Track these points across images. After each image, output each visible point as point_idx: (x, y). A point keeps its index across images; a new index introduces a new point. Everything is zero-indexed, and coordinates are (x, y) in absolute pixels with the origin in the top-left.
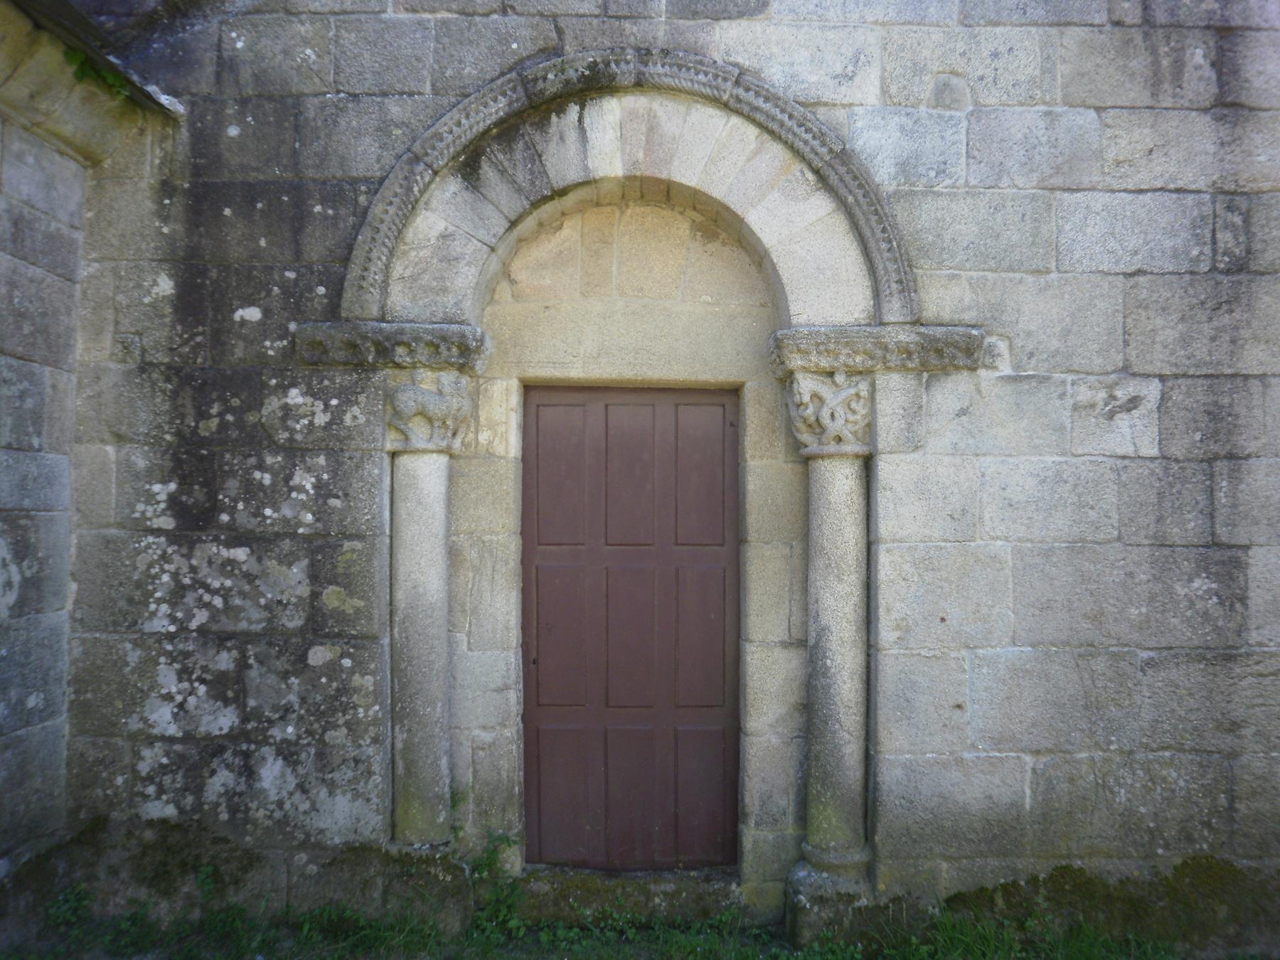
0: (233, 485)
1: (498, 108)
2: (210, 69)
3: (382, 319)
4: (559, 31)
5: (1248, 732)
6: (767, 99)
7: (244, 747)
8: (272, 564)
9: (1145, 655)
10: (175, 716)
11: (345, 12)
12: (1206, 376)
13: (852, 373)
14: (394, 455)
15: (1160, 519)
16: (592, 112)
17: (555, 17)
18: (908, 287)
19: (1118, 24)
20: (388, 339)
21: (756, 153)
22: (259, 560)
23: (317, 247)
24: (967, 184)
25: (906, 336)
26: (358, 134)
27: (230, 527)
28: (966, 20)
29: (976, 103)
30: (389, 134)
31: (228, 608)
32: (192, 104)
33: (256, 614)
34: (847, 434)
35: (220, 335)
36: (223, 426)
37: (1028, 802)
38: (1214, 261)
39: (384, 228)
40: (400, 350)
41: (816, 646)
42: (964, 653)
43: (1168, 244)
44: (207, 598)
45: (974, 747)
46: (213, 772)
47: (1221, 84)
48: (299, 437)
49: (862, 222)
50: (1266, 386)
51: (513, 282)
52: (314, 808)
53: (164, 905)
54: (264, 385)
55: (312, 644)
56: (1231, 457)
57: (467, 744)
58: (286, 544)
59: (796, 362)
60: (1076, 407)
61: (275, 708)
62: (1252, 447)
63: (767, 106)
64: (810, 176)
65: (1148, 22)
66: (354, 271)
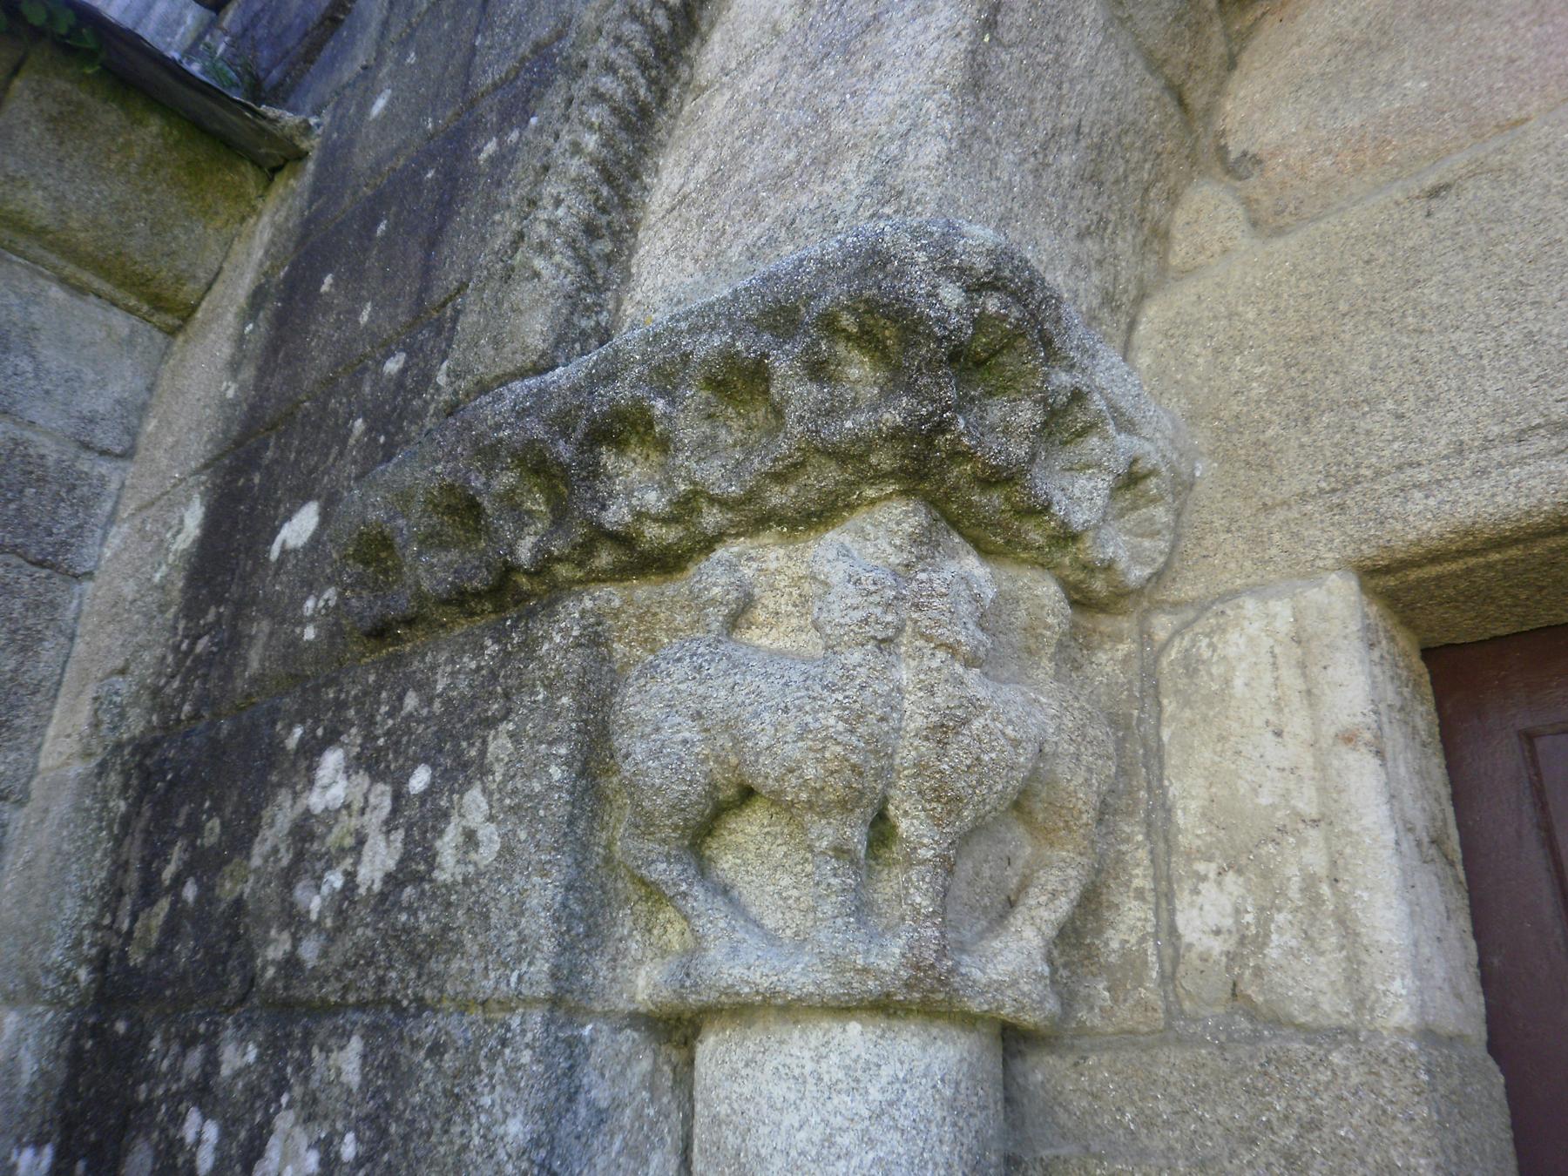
20: (563, 424)
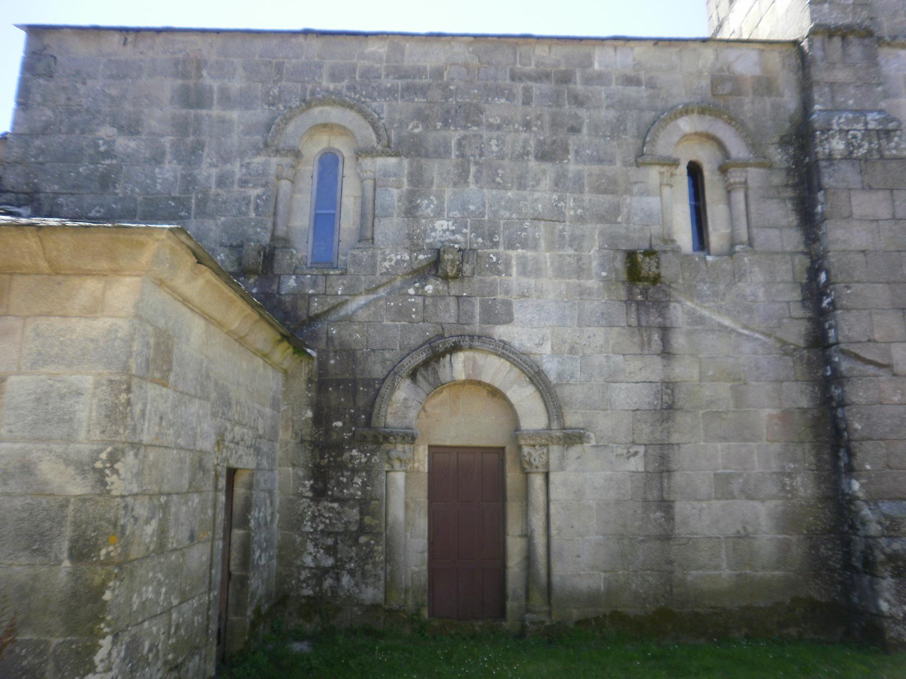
0: (333, 482)
1: (423, 357)
2: (324, 341)
3: (385, 427)
4: (443, 329)
5: (676, 564)
6: (513, 354)
7: (336, 571)
8: (346, 509)
9: (641, 538)
10: (313, 560)
11: (370, 322)
12: (660, 444)
13: (541, 445)
14: (387, 472)
15: (645, 493)
16: (454, 357)
17: (441, 324)
18: (560, 416)
19: (630, 326)
21: (509, 371)
22: (342, 507)
23: (361, 402)
24: (580, 381)
25: (559, 433)
26: (375, 363)
27: (332, 496)
28: (579, 325)
29: (583, 353)
30: (385, 363)
31: (331, 523)
32: (318, 353)
33: (340, 526)
34: (539, 465)
35: (328, 430)
36: (329, 462)
37: (602, 588)
38: (662, 405)
39: (385, 397)
40: (391, 438)
41: (531, 536)
42: (580, 538)
43: (647, 400)
44: (324, 520)
45: (584, 570)
46: (326, 579)
47: (664, 346)
48: (356, 466)
49: (544, 394)
50: (679, 447)
51: (425, 411)
52: (360, 592)
53: (308, 626)
54: (344, 448)
55: (360, 536)
56: (668, 471)
57: (410, 572)
58: (352, 502)
59: (522, 442)
60: (617, 455)
61: (347, 558)
62: (675, 467)
63: (513, 356)
64: (528, 379)
65: (639, 325)
66: (376, 411)
